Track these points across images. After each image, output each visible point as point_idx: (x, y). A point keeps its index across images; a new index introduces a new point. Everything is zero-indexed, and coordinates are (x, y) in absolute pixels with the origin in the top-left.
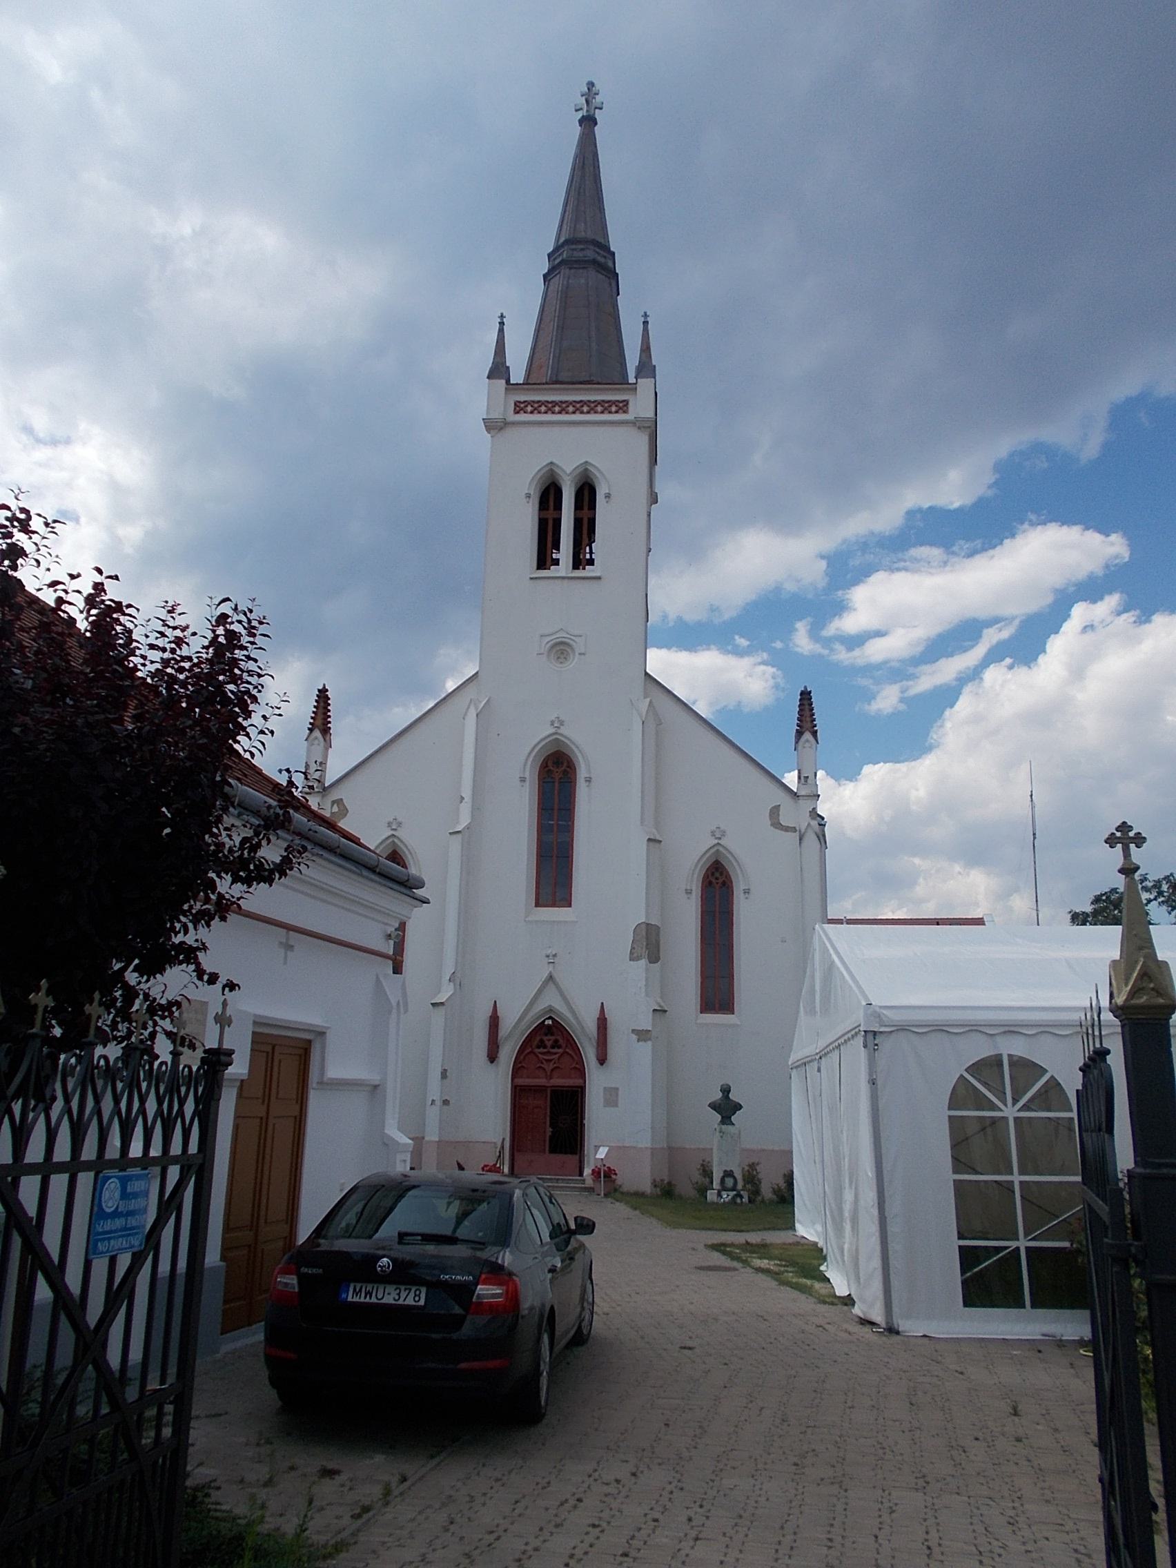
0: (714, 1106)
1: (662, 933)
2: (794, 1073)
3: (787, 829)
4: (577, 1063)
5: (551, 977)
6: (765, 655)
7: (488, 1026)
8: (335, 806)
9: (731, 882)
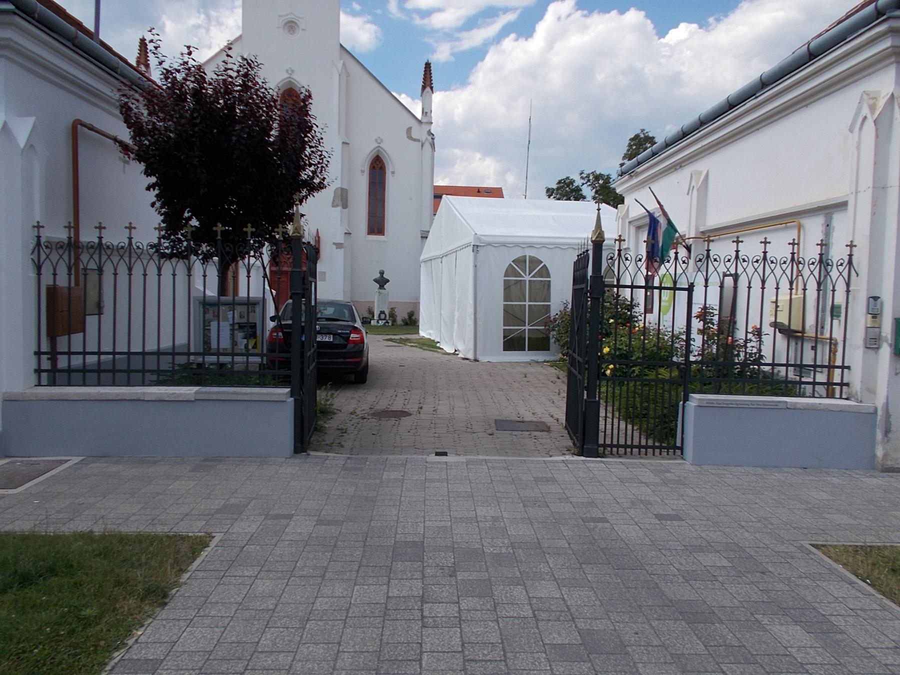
0: (376, 281)
2: (423, 265)
3: (415, 140)
6: (369, 17)
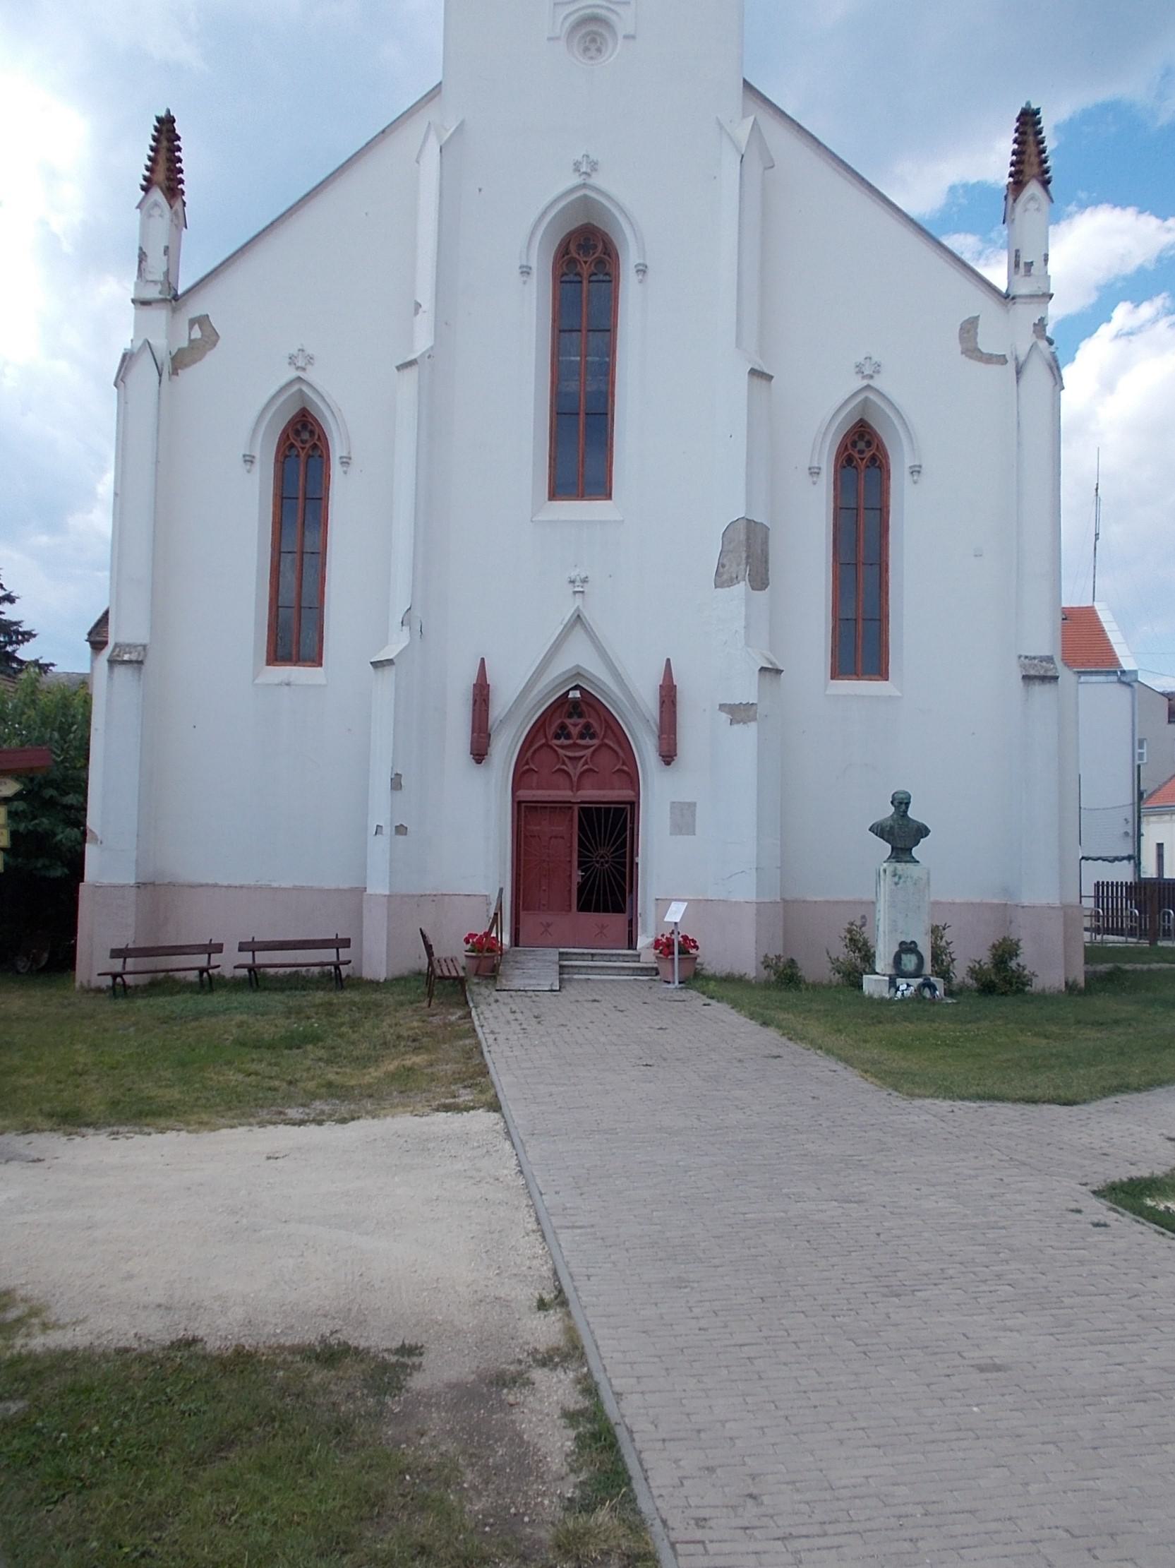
0: (880, 830)
1: (770, 532)
3: (989, 359)
4: (624, 764)
5: (579, 616)
7: (471, 702)
8: (196, 327)
9: (886, 456)
